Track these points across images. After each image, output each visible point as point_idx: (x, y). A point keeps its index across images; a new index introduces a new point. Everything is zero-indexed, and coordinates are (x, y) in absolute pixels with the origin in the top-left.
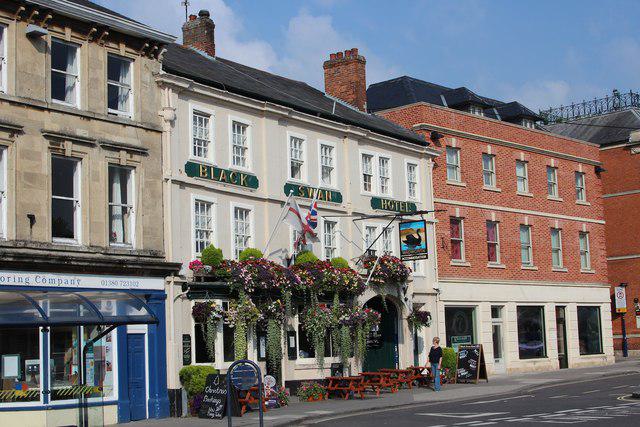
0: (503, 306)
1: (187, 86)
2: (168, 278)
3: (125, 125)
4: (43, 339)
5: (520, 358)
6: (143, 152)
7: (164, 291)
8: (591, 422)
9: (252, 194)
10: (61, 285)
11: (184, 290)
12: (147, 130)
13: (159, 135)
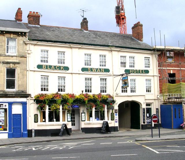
1: (36, 43)
2: (28, 98)
3: (12, 57)
5: (59, 121)
6: (18, 63)
7: (26, 102)
9: (121, 79)
11: (34, 101)
12: (21, 57)
13: (26, 58)
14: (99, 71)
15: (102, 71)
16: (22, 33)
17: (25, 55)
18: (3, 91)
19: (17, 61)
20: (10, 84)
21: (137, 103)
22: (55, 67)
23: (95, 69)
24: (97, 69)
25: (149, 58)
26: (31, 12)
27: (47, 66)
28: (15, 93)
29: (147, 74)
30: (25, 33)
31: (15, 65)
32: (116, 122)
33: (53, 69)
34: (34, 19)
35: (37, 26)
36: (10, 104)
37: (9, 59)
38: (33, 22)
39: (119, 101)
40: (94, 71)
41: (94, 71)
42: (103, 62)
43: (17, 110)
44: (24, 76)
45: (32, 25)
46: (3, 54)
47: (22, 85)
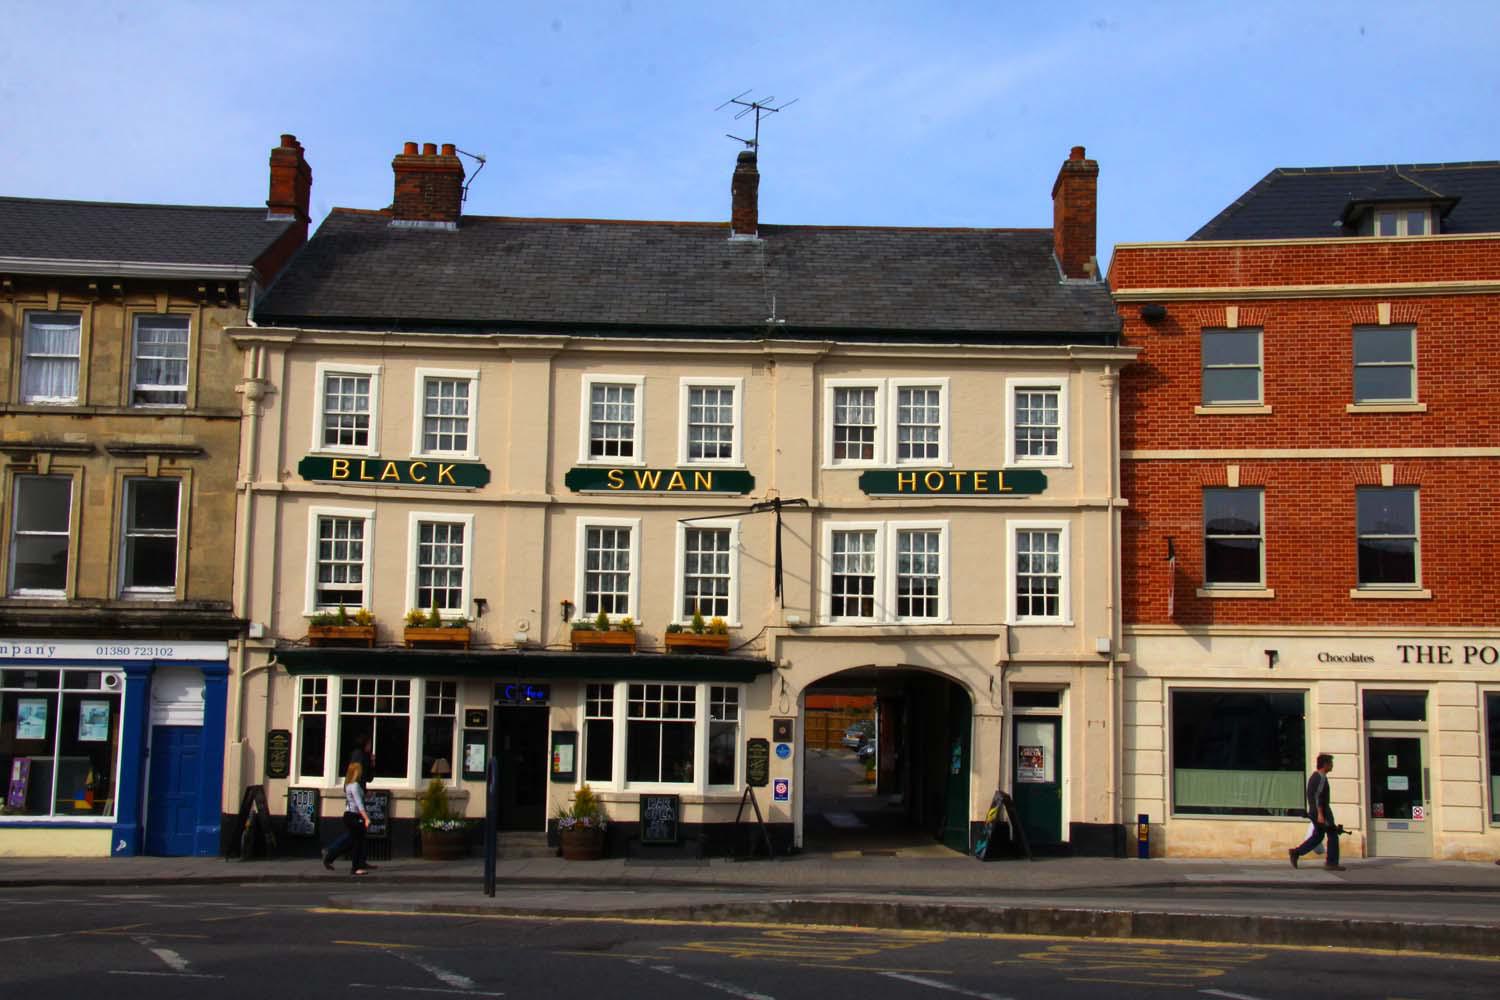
0: (1309, 690)
4: (271, 748)
6: (195, 452)
8: (937, 989)
10: (17, 656)
13: (237, 424)
14: (680, 488)
15: (702, 487)
16: (212, 284)
17: (230, 405)
18: (98, 601)
19: (189, 440)
20: (152, 562)
21: (960, 686)
22: (403, 466)
23: (654, 473)
24: (667, 474)
25: (1058, 388)
26: (412, 147)
27: (355, 464)
28: (166, 613)
29: (1034, 500)
30: (232, 285)
31: (173, 462)
32: (777, 795)
33: (388, 480)
34: (422, 187)
35: (440, 225)
36: (143, 674)
37: (144, 432)
38: (420, 208)
39: (807, 665)
40: (648, 486)
41: (648, 486)
42: (707, 434)
43: (185, 709)
44: (223, 518)
45: (409, 224)
46: (110, 403)
47: (207, 568)
